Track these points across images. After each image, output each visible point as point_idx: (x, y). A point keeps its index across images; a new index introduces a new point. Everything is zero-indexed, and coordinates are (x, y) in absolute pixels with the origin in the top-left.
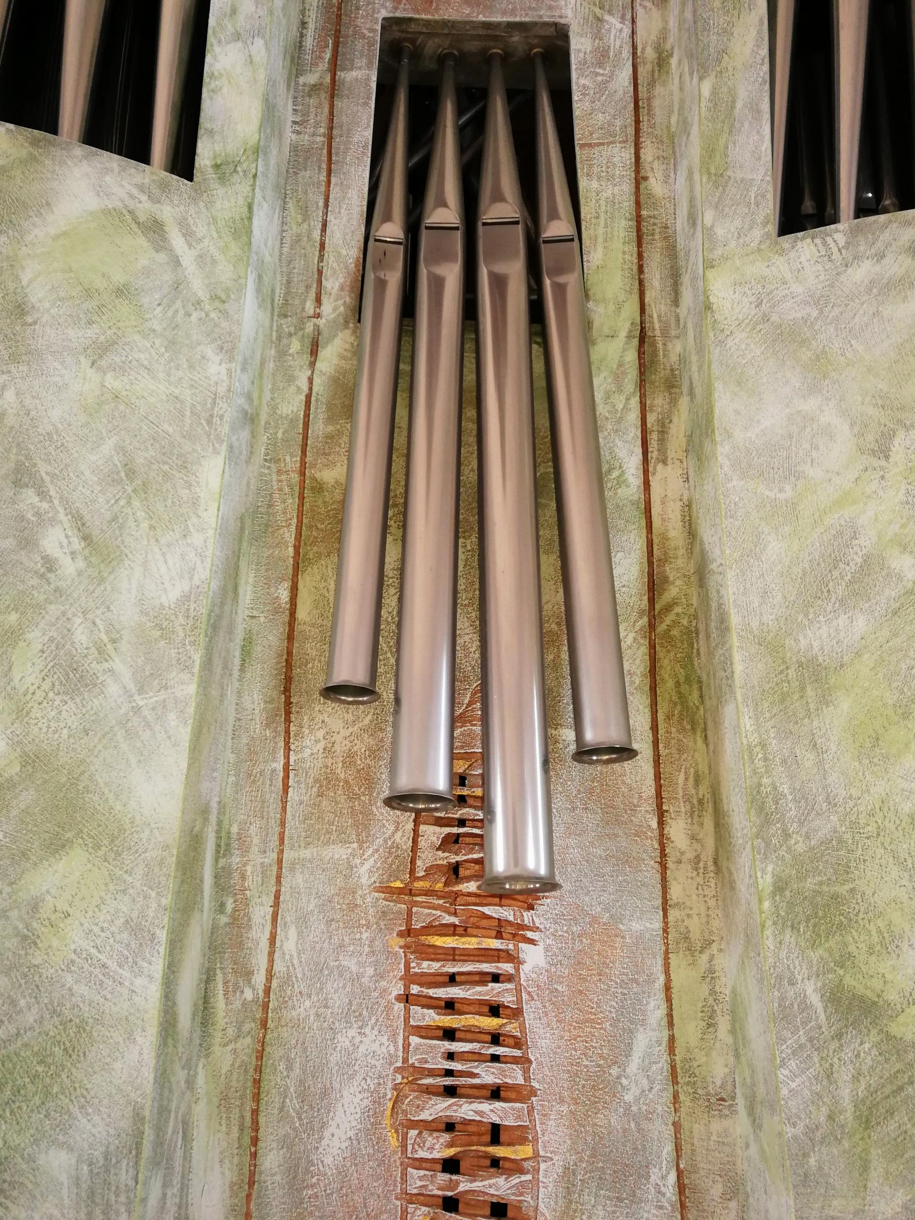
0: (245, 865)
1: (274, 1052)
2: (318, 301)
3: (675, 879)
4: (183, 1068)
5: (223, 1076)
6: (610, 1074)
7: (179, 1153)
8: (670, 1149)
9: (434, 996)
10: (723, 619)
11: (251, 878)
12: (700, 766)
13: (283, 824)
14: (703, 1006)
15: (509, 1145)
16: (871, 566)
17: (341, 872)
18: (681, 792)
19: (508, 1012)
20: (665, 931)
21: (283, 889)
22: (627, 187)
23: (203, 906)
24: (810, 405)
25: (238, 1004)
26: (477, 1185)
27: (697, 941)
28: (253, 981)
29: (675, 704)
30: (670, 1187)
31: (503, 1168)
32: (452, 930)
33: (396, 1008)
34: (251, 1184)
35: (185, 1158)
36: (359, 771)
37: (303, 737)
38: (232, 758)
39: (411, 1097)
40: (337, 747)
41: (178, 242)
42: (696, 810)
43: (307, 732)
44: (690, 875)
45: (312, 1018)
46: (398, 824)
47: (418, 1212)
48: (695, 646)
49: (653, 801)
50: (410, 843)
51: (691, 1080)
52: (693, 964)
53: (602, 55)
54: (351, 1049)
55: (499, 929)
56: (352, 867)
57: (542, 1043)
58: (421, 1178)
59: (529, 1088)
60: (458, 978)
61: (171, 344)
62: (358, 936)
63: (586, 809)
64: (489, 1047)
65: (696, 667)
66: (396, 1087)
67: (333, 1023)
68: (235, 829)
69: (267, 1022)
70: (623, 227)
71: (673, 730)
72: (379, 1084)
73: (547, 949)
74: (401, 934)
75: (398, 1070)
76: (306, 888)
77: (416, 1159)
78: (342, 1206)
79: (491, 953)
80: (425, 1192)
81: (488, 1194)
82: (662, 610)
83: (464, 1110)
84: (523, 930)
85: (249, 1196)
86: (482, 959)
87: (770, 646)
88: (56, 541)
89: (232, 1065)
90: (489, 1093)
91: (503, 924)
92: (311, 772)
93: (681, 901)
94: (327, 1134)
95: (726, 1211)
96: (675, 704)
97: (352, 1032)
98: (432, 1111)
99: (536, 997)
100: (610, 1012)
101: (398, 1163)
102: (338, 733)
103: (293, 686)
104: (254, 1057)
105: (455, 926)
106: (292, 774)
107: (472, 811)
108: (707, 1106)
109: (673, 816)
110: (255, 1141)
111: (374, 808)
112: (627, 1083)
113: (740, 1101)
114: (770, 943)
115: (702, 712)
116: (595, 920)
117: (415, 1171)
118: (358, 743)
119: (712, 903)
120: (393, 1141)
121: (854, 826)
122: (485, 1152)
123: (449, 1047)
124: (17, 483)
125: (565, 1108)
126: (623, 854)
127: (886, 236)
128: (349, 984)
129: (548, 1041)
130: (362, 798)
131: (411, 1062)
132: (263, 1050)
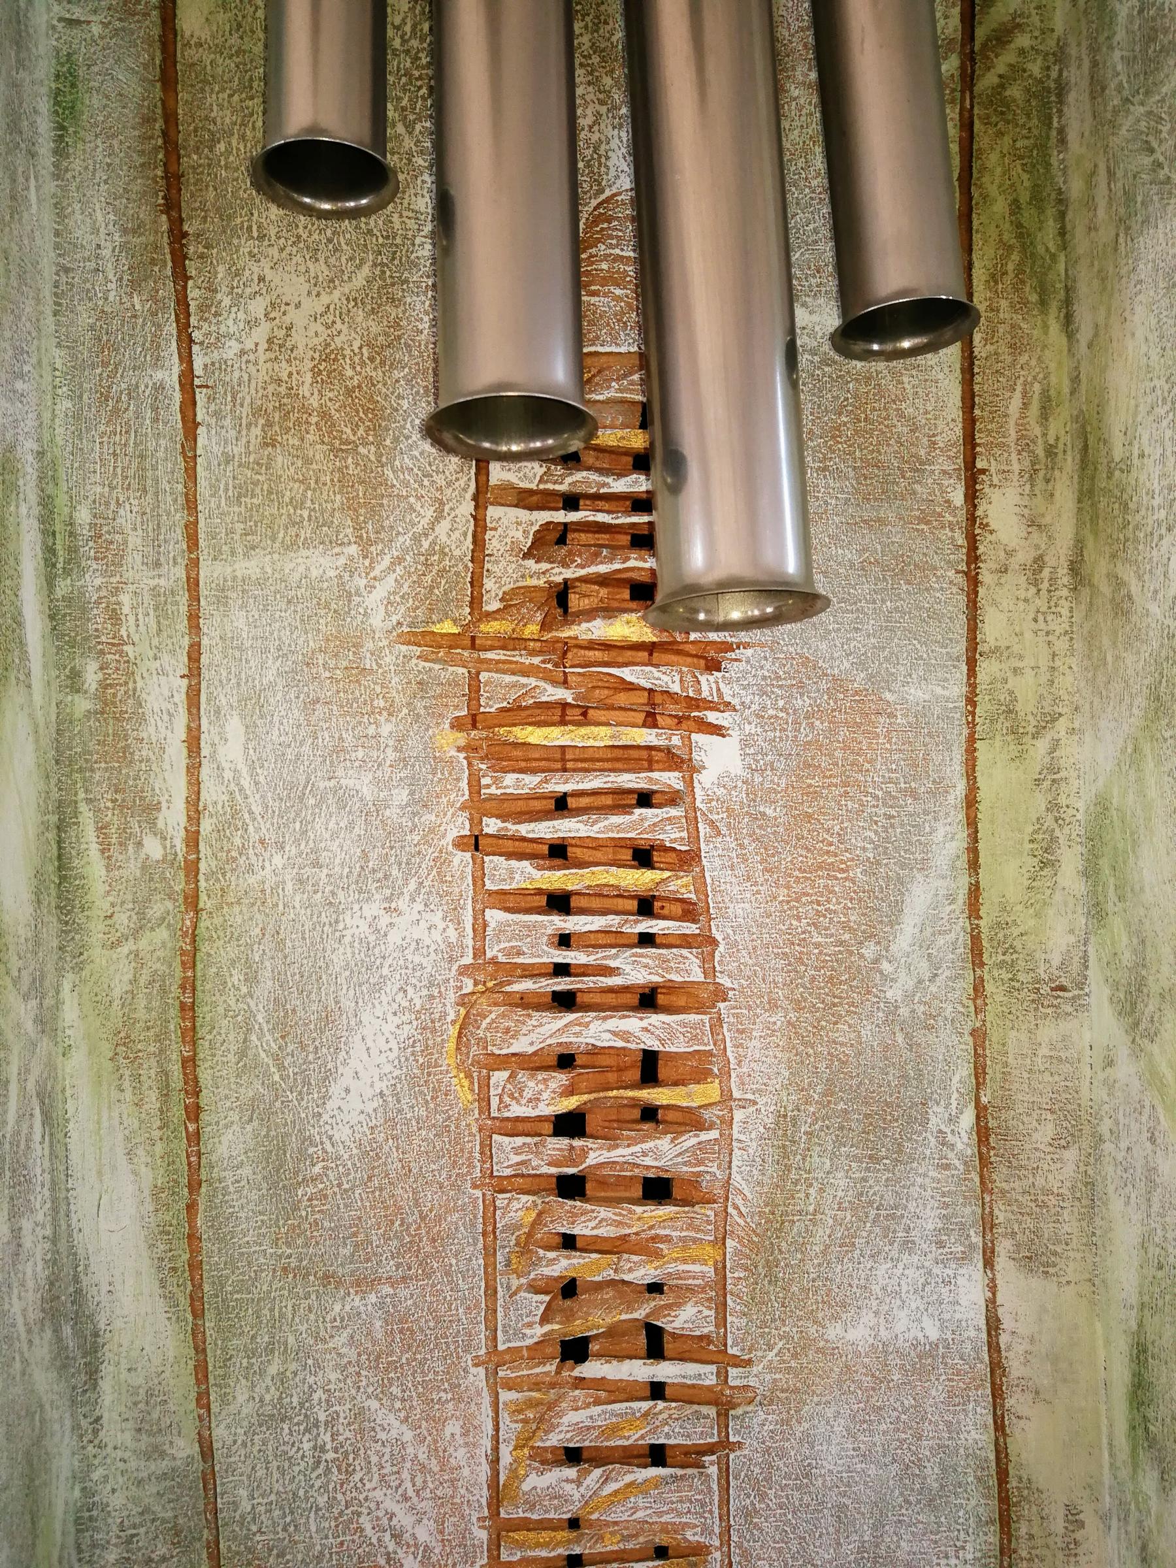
0: (116, 591)
1: (217, 953)
3: (995, 603)
4: (26, 997)
5: (117, 1002)
6: (862, 956)
7: (40, 1150)
8: (965, 1073)
9: (531, 836)
11: (131, 619)
12: (1053, 379)
13: (191, 504)
14: (1036, 832)
15: (676, 1084)
17: (327, 606)
18: (1013, 432)
19: (671, 858)
20: (971, 701)
21: (205, 641)
23: (28, 675)
25: (133, 869)
26: (621, 1153)
27: (1030, 718)
28: (160, 824)
29: (1010, 248)
30: (963, 1134)
31: (664, 1122)
32: (561, 714)
33: (456, 861)
34: (194, 1186)
35: (53, 1155)
36: (349, 392)
37: (216, 314)
38: (59, 357)
39: (493, 1016)
40: (298, 338)
42: (1039, 472)
43: (227, 301)
44: (1022, 594)
45: (289, 886)
46: (442, 503)
47: (516, 1205)
48: (1055, 124)
49: (958, 452)
50: (469, 543)
51: (1007, 958)
52: (1020, 757)
54: (372, 938)
56: (350, 595)
57: (738, 910)
58: (517, 1151)
59: (711, 988)
60: (572, 802)
62: (371, 730)
63: (825, 469)
64: (636, 922)
65: (1055, 170)
66: (462, 1001)
67: (333, 893)
68: (83, 516)
69: (197, 897)
71: (1004, 304)
72: (431, 997)
73: (745, 743)
74: (457, 725)
75: (464, 971)
76: (255, 638)
77: (508, 1119)
78: (373, 1207)
79: (635, 754)
80: (525, 1171)
81: (638, 1166)
82: (989, 39)
83: (597, 1031)
84: (698, 708)
85: (191, 1207)
86: (619, 765)
89: (135, 980)
90: (635, 1000)
91: (658, 699)
92: (244, 393)
93: (1003, 644)
94: (335, 1089)
95: (1059, 1165)
96: (1010, 248)
97: (372, 909)
98: (533, 1037)
99: (724, 830)
100: (864, 849)
101: (474, 1130)
102: (298, 305)
103: (185, 196)
104: (177, 963)
105: (564, 706)
106: (201, 397)
107: (594, 477)
108: (1033, 1001)
109: (995, 481)
110: (194, 1112)
111: (389, 473)
112: (891, 969)
113: (1099, 993)
115: (1061, 267)
116: (838, 684)
117: (507, 1139)
118: (344, 328)
119: (1061, 645)
120: (463, 1093)
122: (633, 1099)
123: (563, 925)
125: (778, 1018)
126: (896, 558)
128: (360, 822)
129: (747, 906)
130: (361, 450)
131: (489, 955)
132: (195, 949)
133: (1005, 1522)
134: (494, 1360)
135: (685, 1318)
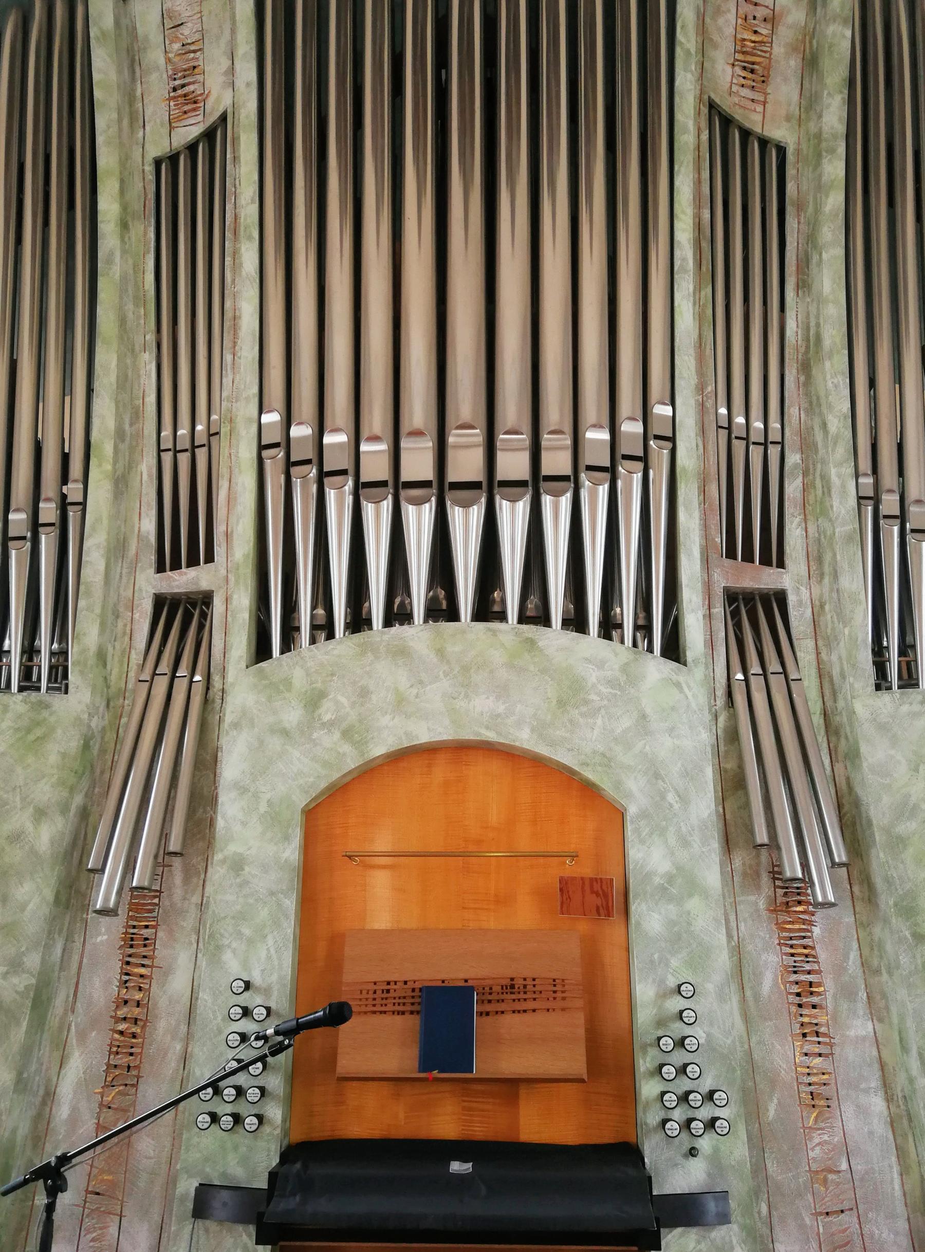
1: (744, 961)
2: (715, 700)
10: (870, 823)
16: (915, 807)
22: (814, 656)
24: (893, 752)
41: (686, 690)
42: (861, 883)
53: (800, 603)
55: (804, 922)
61: (690, 727)
70: (814, 672)
83: (803, 977)
87: (887, 831)
88: (671, 797)
113: (884, 971)
114: (894, 921)
121: (916, 886)
124: (657, 779)
127: (913, 696)
133: (882, 1070)
134: (792, 1035)
135: (823, 1030)
